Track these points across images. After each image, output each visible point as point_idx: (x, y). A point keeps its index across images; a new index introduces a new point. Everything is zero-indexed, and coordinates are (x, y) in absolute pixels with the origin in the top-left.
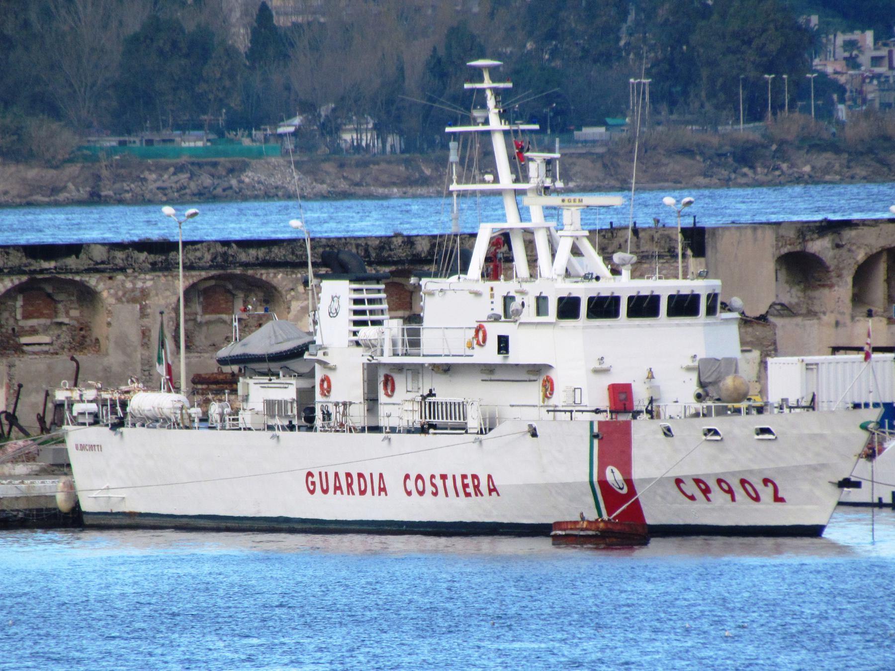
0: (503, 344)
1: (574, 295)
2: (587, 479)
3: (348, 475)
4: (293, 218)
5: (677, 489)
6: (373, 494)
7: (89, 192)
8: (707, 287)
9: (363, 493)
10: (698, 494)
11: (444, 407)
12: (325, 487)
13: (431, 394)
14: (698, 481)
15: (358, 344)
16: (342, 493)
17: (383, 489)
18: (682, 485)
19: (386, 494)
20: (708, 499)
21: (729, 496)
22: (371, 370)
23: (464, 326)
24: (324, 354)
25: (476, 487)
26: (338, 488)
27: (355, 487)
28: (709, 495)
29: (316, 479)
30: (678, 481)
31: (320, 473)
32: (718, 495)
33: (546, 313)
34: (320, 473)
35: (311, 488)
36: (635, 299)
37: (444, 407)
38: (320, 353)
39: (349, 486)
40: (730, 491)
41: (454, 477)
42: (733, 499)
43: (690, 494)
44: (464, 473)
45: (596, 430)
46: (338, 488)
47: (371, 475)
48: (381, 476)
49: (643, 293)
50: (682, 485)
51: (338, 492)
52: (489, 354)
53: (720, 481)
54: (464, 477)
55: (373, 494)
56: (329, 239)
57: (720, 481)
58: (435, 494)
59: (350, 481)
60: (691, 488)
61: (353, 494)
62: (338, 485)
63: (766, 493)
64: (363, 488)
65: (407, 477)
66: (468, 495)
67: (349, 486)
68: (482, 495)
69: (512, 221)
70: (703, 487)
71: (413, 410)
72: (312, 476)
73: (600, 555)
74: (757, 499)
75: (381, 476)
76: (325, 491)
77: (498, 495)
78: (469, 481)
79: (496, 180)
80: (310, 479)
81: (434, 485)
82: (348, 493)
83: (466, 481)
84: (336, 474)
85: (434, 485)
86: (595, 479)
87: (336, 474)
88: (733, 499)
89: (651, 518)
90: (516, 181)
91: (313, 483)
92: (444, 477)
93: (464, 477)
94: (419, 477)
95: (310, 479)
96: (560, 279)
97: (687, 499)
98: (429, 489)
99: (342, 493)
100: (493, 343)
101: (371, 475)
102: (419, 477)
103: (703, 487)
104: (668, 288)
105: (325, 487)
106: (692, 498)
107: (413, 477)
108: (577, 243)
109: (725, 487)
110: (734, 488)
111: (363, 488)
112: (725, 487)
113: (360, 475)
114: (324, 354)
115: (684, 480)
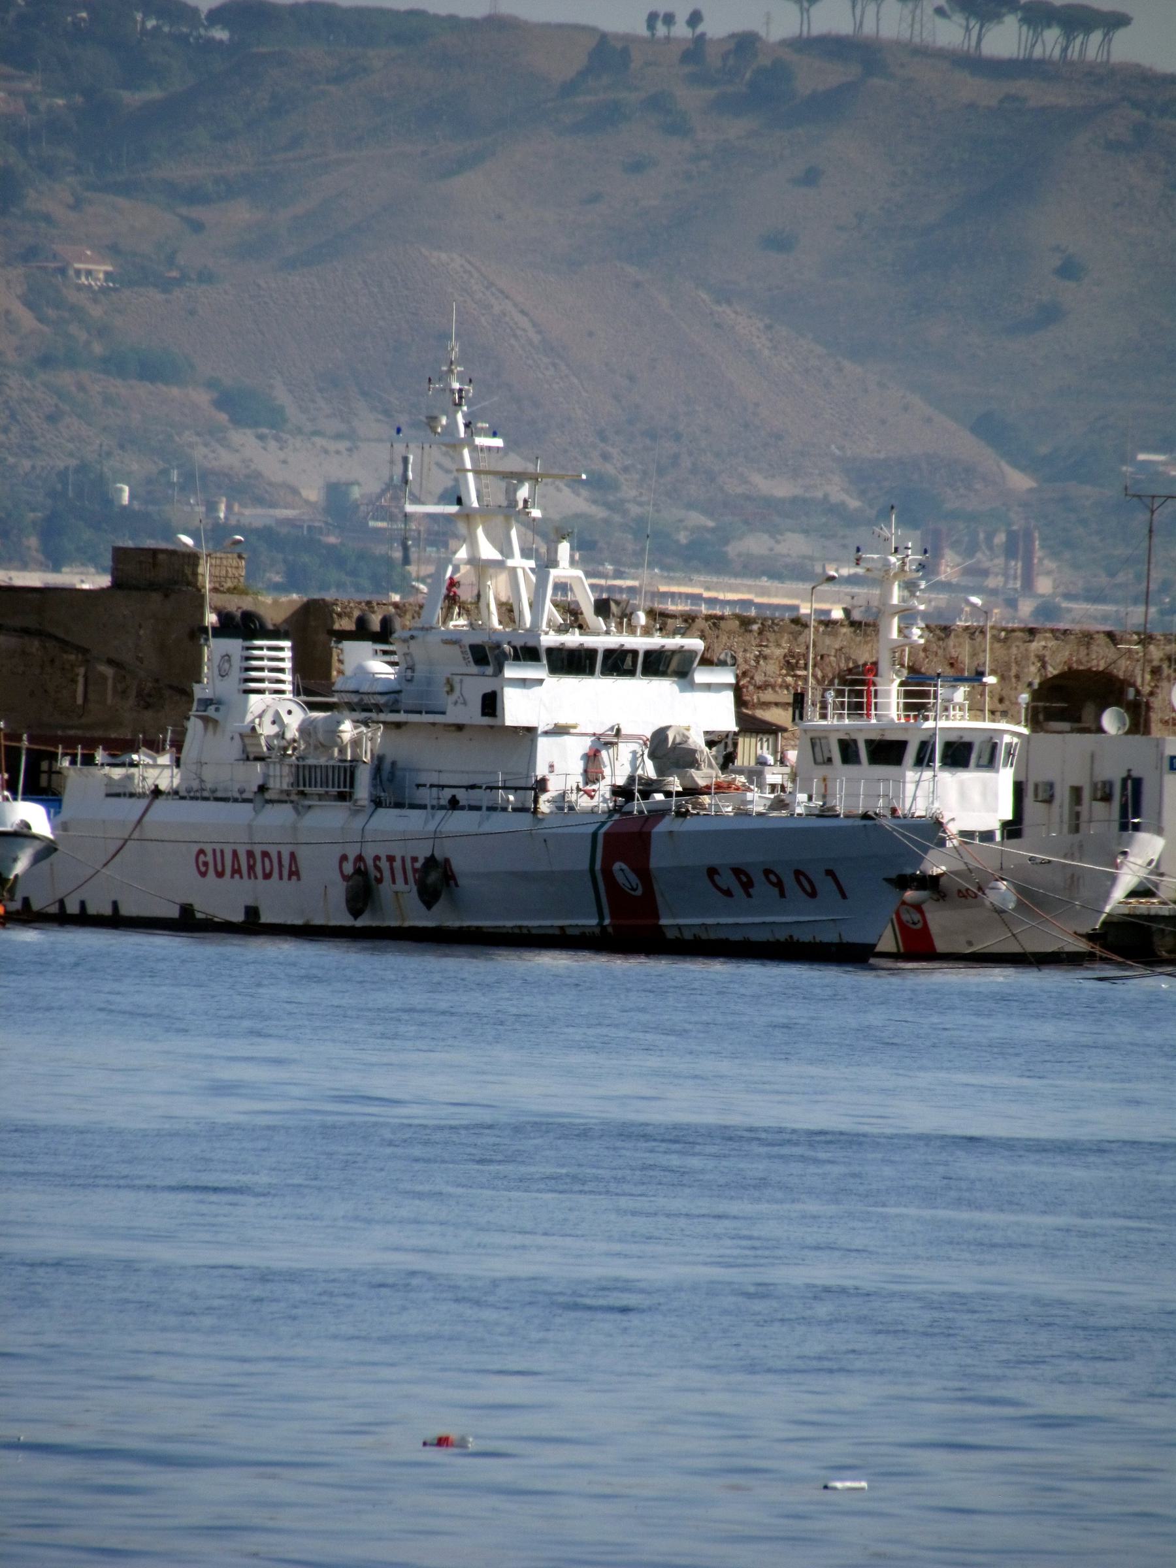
2: (586, 865)
5: (338, 861)
9: (267, 876)
11: (336, 771)
12: (220, 869)
13: (578, 789)
14: (737, 872)
16: (241, 877)
17: (294, 873)
18: (716, 877)
19: (299, 879)
20: (749, 895)
21: (776, 891)
26: (236, 871)
29: (210, 859)
30: (712, 872)
31: (214, 851)
32: (761, 888)
35: (203, 869)
36: (655, 655)
37: (336, 771)
39: (251, 868)
40: (779, 885)
41: (403, 859)
42: (782, 894)
43: (725, 887)
44: (414, 855)
46: (236, 871)
48: (293, 856)
50: (716, 877)
51: (294, 878)
53: (767, 872)
55: (281, 878)
57: (767, 872)
59: (252, 863)
60: (727, 880)
61: (256, 878)
62: (236, 867)
63: (825, 886)
67: (251, 868)
70: (744, 879)
71: (1109, 821)
72: (205, 855)
74: (813, 894)
75: (293, 856)
76: (220, 875)
82: (250, 877)
86: (598, 866)
87: (235, 854)
88: (782, 894)
91: (206, 864)
99: (241, 877)
103: (744, 879)
105: (220, 869)
106: (728, 893)
109: (773, 878)
112: (773, 878)
113: (265, 854)
114: (217, 710)
115: (720, 870)
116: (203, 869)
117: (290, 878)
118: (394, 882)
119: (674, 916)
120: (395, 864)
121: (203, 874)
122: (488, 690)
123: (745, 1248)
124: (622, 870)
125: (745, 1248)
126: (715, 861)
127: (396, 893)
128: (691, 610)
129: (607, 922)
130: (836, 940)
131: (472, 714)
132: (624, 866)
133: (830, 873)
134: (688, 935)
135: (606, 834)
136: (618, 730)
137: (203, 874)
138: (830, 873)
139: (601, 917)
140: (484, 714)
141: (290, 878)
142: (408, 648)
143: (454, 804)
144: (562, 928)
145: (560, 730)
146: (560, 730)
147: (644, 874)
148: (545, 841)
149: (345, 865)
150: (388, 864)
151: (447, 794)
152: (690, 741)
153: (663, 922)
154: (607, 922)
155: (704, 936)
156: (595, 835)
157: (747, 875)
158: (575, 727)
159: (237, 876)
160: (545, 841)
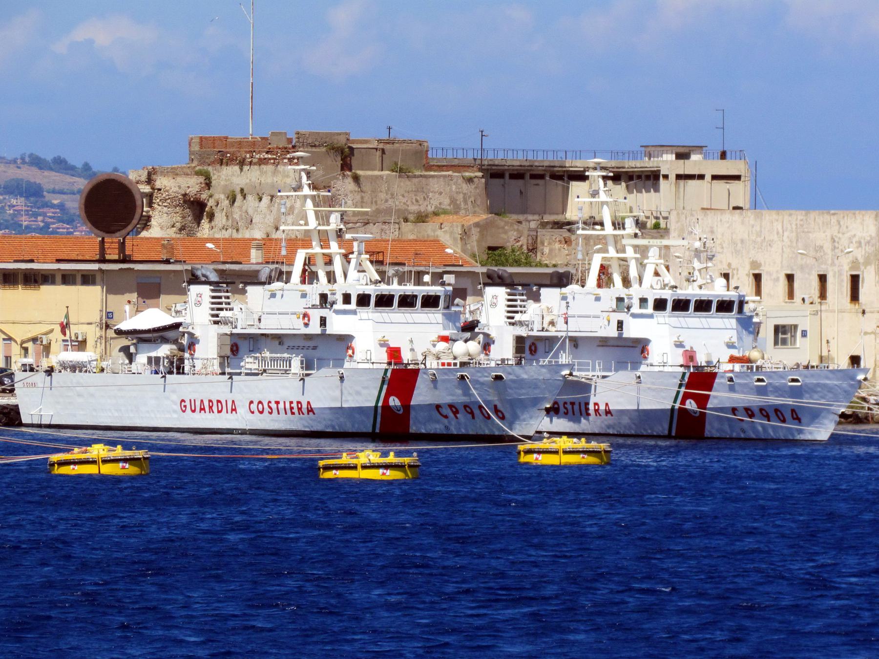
0: (323, 321)
1: (366, 293)
3: (210, 401)
6: (227, 412)
8: (375, 290)
9: (219, 412)
10: (451, 415)
14: (451, 406)
15: (513, 324)
17: (234, 410)
18: (440, 409)
21: (471, 416)
22: (520, 341)
23: (277, 311)
24: (193, 328)
25: (300, 409)
26: (202, 409)
27: (215, 408)
28: (458, 415)
29: (188, 403)
30: (438, 407)
33: (646, 308)
34: (190, 400)
35: (184, 409)
38: (190, 328)
39: (211, 408)
40: (472, 413)
42: (473, 417)
45: (389, 374)
47: (226, 401)
48: (233, 402)
49: (703, 298)
50: (440, 409)
51: (234, 412)
52: (315, 328)
53: (793, 411)
54: (291, 403)
55: (227, 412)
58: (271, 413)
64: (220, 409)
65: (251, 402)
66: (293, 413)
67: (211, 408)
68: (600, 415)
69: (317, 249)
70: (454, 410)
75: (233, 402)
77: (314, 414)
78: (294, 405)
79: (306, 224)
81: (270, 408)
83: (292, 405)
84: (202, 401)
85: (270, 408)
86: (380, 404)
87: (202, 401)
88: (473, 417)
90: (615, 229)
91: (185, 406)
93: (291, 403)
94: (260, 402)
95: (183, 404)
96: (300, 284)
98: (267, 409)
100: (614, 325)
101: (226, 401)
102: (260, 402)
103: (454, 410)
104: (423, 291)
105: (193, 409)
107: (255, 403)
108: (657, 268)
109: (765, 414)
110: (770, 414)
111: (220, 409)
112: (765, 414)
121: (184, 411)
123: (675, 563)
125: (675, 563)
128: (156, 349)
137: (184, 411)
142: (666, 177)
147: (406, 406)
148: (790, 278)
149: (252, 405)
152: (873, 216)
157: (456, 408)
160: (790, 278)
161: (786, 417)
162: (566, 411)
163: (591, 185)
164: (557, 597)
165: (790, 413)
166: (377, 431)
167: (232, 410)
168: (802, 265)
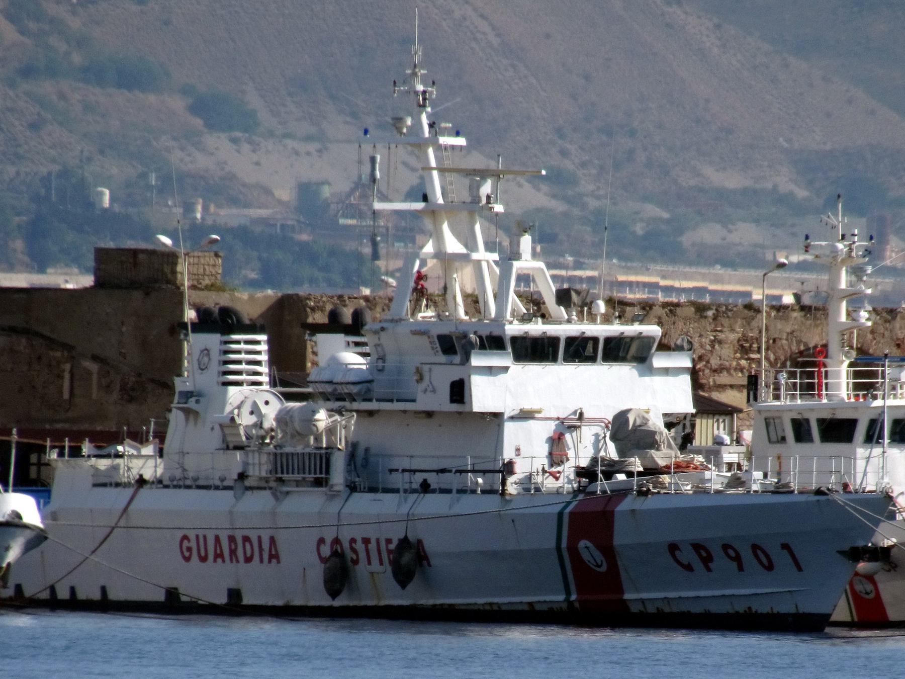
2: (552, 544)
4: (417, 295)
7: (434, 292)
9: (248, 560)
10: (697, 564)
11: (312, 459)
12: (203, 554)
14: (697, 547)
16: (224, 561)
17: (274, 556)
18: (677, 553)
19: (279, 562)
20: (709, 570)
21: (734, 565)
26: (219, 555)
29: (193, 544)
30: (673, 548)
31: (197, 537)
32: (721, 562)
35: (187, 554)
39: (233, 552)
40: (738, 559)
41: (378, 541)
42: (741, 568)
43: (685, 562)
44: (389, 537)
46: (219, 555)
48: (272, 540)
51: (219, 560)
53: (726, 547)
55: (261, 561)
56: (627, 325)
60: (688, 555)
61: (238, 561)
62: (218, 552)
63: (782, 559)
67: (233, 552)
70: (704, 554)
73: (843, 630)
74: (770, 567)
75: (272, 540)
76: (203, 559)
80: (186, 543)
82: (231, 561)
86: (564, 544)
87: (217, 539)
88: (741, 568)
89: (247, 600)
92: (366, 541)
93: (232, 539)
97: (680, 568)
99: (224, 561)
103: (704, 554)
105: (203, 554)
106: (689, 568)
113: (246, 539)
114: (197, 402)
116: (187, 554)
117: (270, 562)
118: (369, 563)
119: (638, 590)
120: (370, 546)
121: (187, 559)
122: (456, 378)
124: (587, 548)
126: (675, 537)
127: (372, 573)
129: (574, 597)
130: (792, 610)
131: (441, 401)
132: (589, 544)
133: (786, 547)
134: (651, 609)
135: (571, 514)
136: (581, 414)
137: (187, 559)
138: (786, 547)
139: (568, 593)
140: (453, 401)
141: (270, 562)
143: (425, 487)
144: (530, 604)
145: (525, 415)
146: (525, 415)
147: (608, 550)
149: (322, 548)
150: (363, 546)
151: (419, 478)
153: (627, 596)
154: (574, 597)
155: (667, 610)
156: (560, 515)
158: (539, 412)
159: (219, 560)
161: (752, 557)
162: (354, 545)
163: (139, 471)
164: (283, 647)
165: (750, 551)
166: (856, 619)
167: (271, 557)
168: (857, 387)
